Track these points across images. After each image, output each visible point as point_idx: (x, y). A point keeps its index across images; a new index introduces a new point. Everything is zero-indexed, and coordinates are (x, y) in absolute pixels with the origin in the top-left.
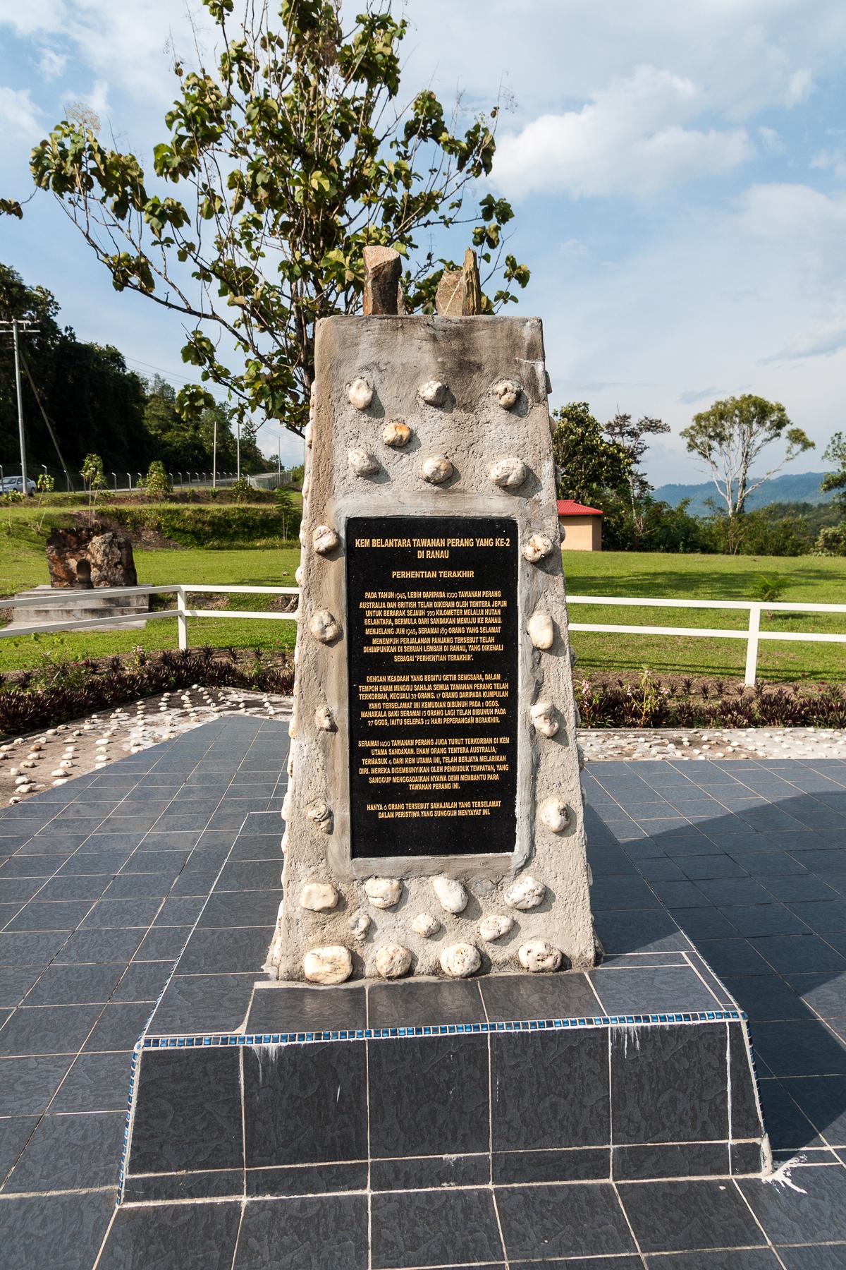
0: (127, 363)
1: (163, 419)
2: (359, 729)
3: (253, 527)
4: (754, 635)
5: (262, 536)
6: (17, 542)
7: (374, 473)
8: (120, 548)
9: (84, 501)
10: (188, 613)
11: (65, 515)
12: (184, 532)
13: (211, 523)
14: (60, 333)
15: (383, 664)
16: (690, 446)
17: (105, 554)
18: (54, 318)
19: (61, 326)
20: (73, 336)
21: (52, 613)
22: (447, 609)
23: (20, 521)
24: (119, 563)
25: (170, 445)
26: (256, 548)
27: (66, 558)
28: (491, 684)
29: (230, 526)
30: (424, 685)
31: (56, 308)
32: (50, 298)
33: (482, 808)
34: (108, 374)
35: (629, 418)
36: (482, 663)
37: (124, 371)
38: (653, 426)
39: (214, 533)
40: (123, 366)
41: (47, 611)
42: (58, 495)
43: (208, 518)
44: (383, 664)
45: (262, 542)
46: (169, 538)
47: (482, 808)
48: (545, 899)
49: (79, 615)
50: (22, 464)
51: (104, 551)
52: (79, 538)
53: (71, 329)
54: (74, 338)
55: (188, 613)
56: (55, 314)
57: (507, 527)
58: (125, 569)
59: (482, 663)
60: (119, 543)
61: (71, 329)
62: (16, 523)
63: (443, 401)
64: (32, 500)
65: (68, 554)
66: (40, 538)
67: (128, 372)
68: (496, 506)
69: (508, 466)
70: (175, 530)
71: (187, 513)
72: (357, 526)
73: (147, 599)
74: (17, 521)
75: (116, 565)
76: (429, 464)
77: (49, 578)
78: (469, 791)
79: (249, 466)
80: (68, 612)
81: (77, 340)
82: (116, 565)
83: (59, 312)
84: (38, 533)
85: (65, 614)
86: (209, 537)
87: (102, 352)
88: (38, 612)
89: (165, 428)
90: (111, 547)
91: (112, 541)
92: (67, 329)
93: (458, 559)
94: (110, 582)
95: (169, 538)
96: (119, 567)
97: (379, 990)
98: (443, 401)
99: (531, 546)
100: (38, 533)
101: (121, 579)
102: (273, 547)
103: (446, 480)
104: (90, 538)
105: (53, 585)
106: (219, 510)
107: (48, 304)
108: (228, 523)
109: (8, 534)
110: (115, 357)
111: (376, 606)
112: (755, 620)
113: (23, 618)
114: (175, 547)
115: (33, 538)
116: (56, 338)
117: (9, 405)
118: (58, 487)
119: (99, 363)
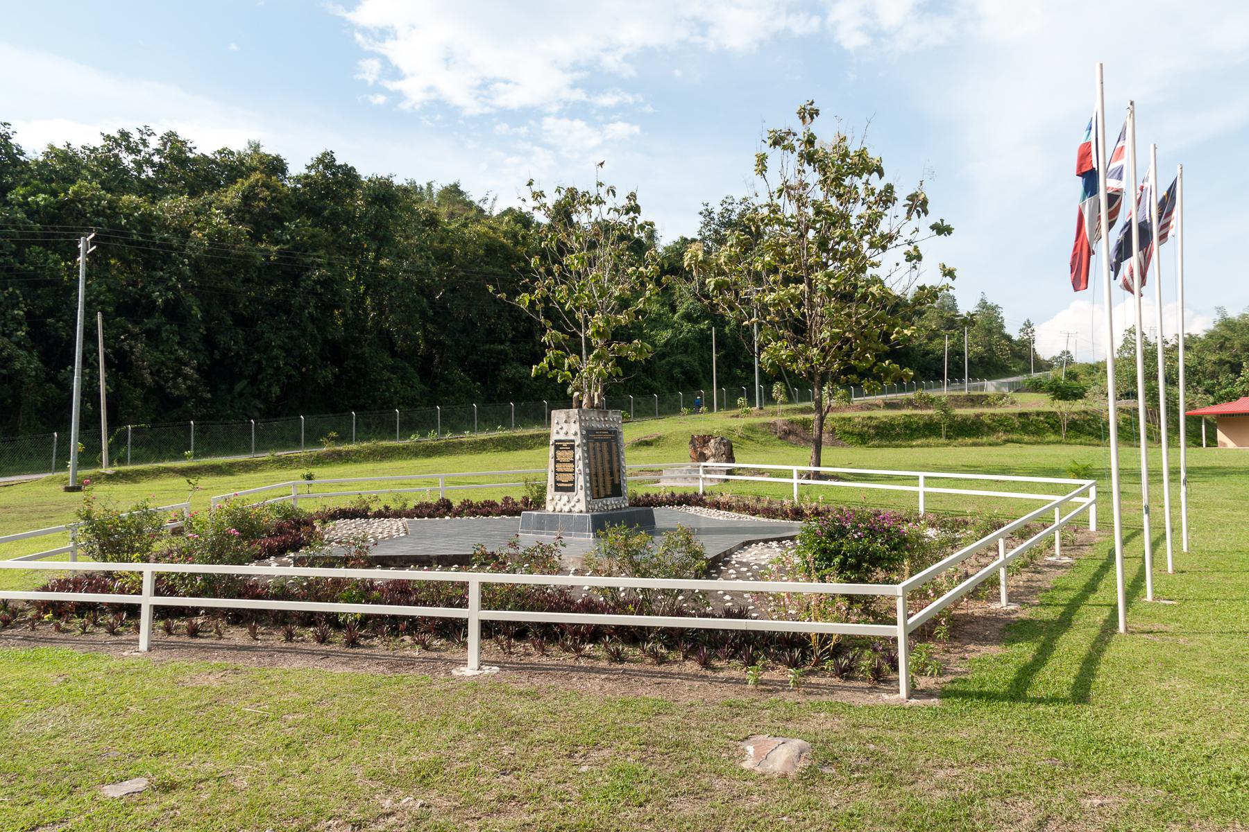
2: (556, 472)
3: (916, 430)
4: (921, 489)
5: (969, 436)
7: (558, 433)
9: (774, 414)
10: (703, 476)
12: (851, 434)
13: (876, 427)
15: (558, 462)
22: (567, 453)
25: (933, 353)
26: (983, 445)
28: (572, 465)
29: (894, 429)
30: (564, 465)
33: (571, 485)
36: (571, 462)
39: (877, 434)
42: (790, 406)
43: (874, 423)
44: (558, 462)
45: (919, 442)
46: (840, 439)
47: (571, 485)
48: (579, 501)
55: (703, 476)
57: (573, 441)
59: (571, 462)
63: (566, 422)
64: (761, 412)
68: (572, 438)
69: (573, 432)
70: (845, 432)
71: (856, 420)
72: (556, 441)
76: (564, 431)
78: (570, 482)
79: (1021, 366)
86: (872, 438)
93: (568, 446)
95: (840, 439)
98: (566, 422)
99: (577, 443)
102: (928, 446)
103: (567, 433)
106: (886, 417)
108: (892, 426)
111: (559, 453)
112: (921, 481)
114: (843, 446)
118: (790, 399)
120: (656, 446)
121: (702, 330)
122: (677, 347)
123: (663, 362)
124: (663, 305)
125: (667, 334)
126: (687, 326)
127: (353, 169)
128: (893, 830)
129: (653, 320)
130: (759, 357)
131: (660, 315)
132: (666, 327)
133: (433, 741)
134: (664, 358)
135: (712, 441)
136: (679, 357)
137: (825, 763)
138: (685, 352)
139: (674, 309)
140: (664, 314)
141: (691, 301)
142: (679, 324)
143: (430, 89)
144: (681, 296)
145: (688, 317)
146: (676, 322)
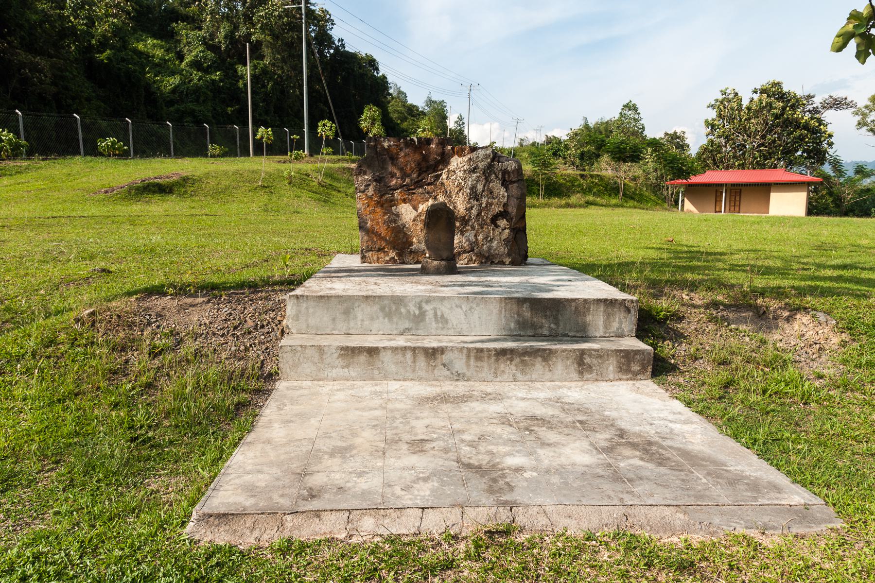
0: (380, 68)
1: (401, 113)
6: (298, 192)
8: (505, 184)
11: (344, 169)
14: (334, 44)
16: (859, 124)
17: (474, 195)
18: (330, 32)
19: (336, 38)
20: (343, 45)
21: (386, 358)
23: (302, 171)
24: (503, 214)
27: (392, 202)
31: (332, 24)
32: (328, 17)
34: (366, 75)
35: (812, 97)
37: (377, 73)
38: (837, 104)
40: (377, 69)
41: (373, 352)
42: (334, 157)
49: (460, 365)
50: (305, 130)
51: (473, 188)
52: (425, 158)
53: (343, 40)
54: (344, 47)
56: (331, 29)
58: (513, 229)
60: (505, 172)
61: (343, 40)
62: (298, 173)
65: (397, 194)
66: (321, 189)
67: (380, 74)
73: (633, 317)
74: (299, 172)
75: (494, 220)
77: (358, 239)
80: (432, 353)
81: (347, 49)
82: (494, 220)
83: (335, 26)
84: (319, 184)
85: (422, 361)
87: (362, 58)
88: (349, 352)
89: (404, 119)
90: (487, 180)
91: (490, 166)
92: (339, 40)
94: (480, 255)
96: (503, 223)
97: (361, 298)
100: (319, 184)
101: (504, 250)
104: (444, 160)
105: (364, 258)
107: (327, 21)
109: (290, 183)
110: (372, 63)
113: (307, 368)
115: (314, 189)
116: (331, 48)
117: (297, 96)
119: (361, 67)
120: (180, 195)
121: (213, 81)
122: (187, 95)
123: (172, 109)
124: (168, 51)
125: (175, 80)
126: (196, 75)
127: (375, 60)
128: (872, 526)
129: (157, 65)
130: (254, 135)
131: (165, 61)
132: (173, 73)
133: (143, 311)
134: (173, 105)
135: (456, 162)
136: (191, 106)
137: (748, 542)
138: (197, 101)
139: (181, 57)
140: (169, 60)
141: (201, 48)
142: (187, 72)
143: (684, 133)
144: (189, 43)
145: (196, 64)
146: (183, 70)
